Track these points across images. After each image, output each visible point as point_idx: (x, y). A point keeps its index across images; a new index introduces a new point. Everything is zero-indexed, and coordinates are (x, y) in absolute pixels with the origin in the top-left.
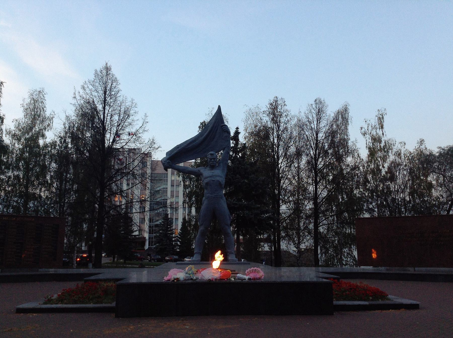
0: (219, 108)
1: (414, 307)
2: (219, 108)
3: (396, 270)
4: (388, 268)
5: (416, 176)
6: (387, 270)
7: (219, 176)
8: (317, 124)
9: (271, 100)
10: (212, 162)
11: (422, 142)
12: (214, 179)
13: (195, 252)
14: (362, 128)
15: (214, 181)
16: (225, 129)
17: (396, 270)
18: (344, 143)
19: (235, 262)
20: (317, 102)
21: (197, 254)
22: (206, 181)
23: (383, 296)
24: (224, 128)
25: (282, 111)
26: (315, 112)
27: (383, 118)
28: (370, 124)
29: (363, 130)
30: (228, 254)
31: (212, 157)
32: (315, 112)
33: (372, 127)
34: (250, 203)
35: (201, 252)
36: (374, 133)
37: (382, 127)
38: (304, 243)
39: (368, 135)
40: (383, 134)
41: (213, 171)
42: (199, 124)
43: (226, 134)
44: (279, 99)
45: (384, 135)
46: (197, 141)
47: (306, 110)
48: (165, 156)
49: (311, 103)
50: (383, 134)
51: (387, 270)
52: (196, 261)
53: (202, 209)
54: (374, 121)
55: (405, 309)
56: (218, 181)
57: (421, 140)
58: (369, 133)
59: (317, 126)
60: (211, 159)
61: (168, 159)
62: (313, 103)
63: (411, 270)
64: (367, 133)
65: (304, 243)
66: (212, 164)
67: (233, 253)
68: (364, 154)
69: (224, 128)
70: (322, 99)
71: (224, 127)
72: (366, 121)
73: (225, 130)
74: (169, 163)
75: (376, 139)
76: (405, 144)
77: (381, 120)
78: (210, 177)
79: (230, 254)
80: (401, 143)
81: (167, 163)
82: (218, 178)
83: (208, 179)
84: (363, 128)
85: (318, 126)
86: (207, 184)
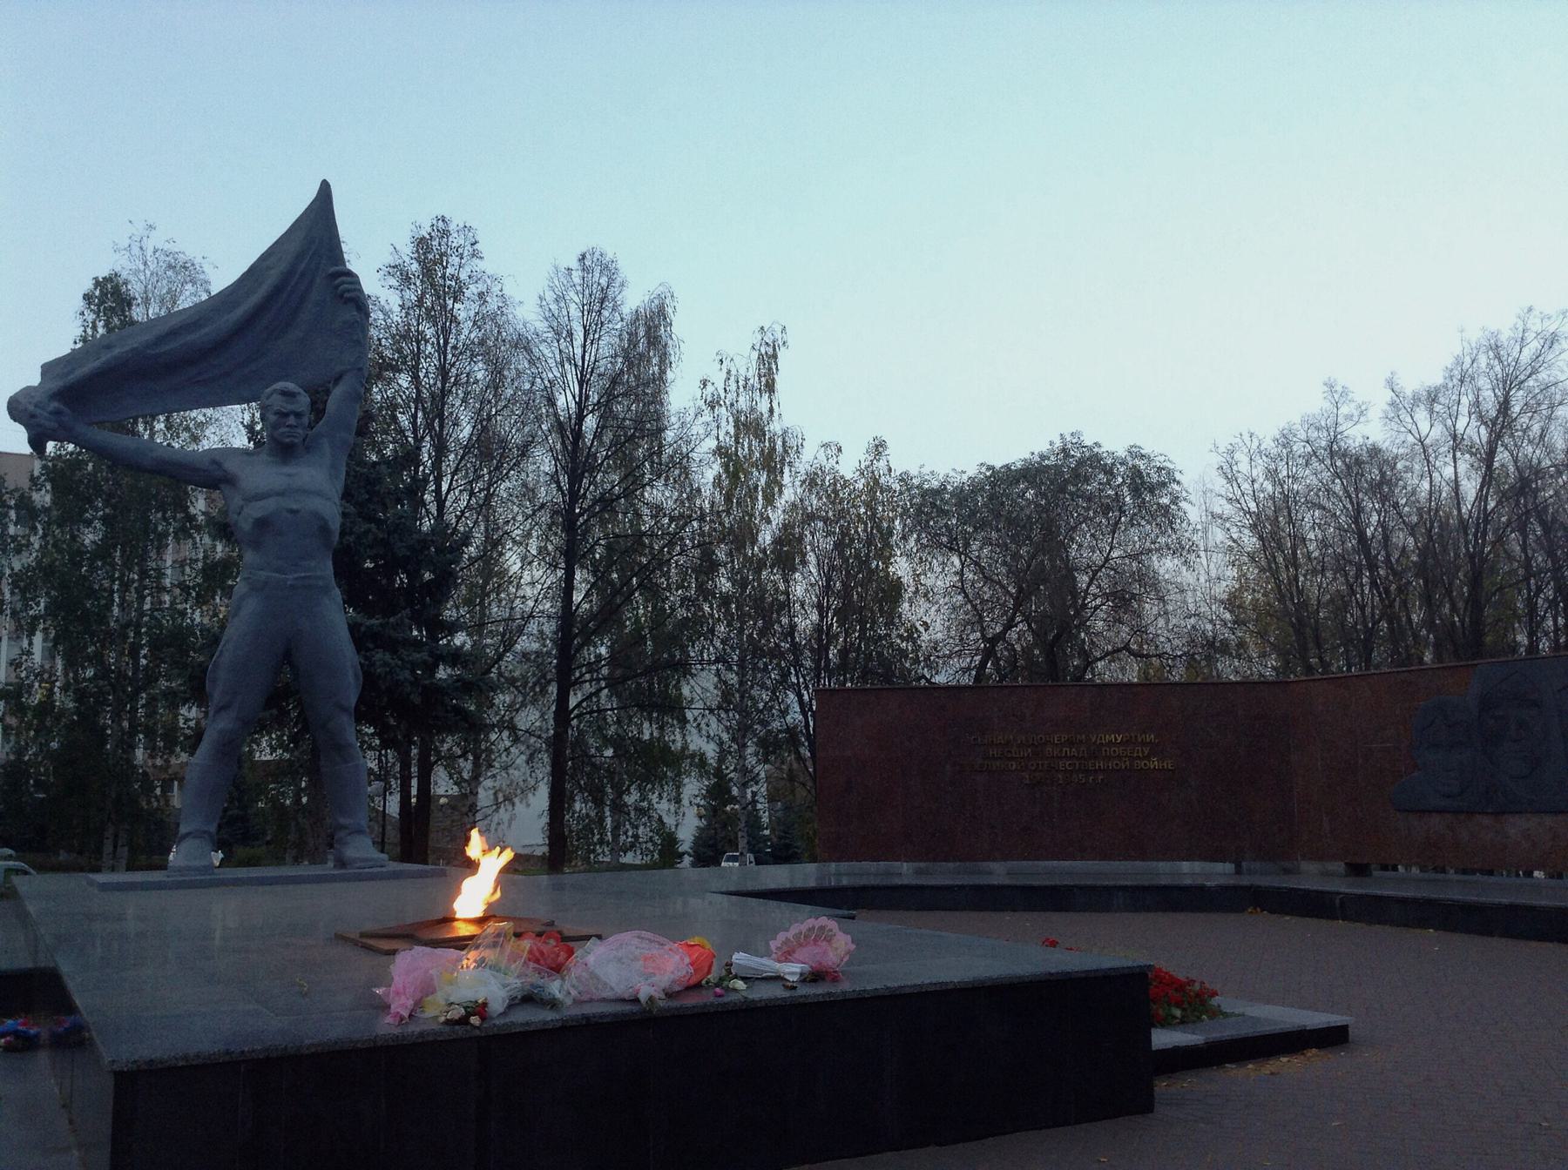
0: (325, 191)
1: (1334, 1038)
2: (325, 191)
3: (944, 874)
4: (922, 865)
5: (858, 556)
6: (918, 872)
7: (319, 494)
8: (584, 346)
9: (423, 225)
10: (287, 429)
11: (879, 448)
12: (295, 507)
13: (183, 830)
14: (704, 383)
15: (292, 512)
16: (349, 291)
17: (944, 874)
18: (650, 423)
19: (379, 869)
20: (588, 263)
21: (194, 837)
22: (256, 511)
23: (1195, 1003)
24: (343, 283)
25: (463, 276)
26: (577, 300)
27: (775, 356)
28: (734, 372)
29: (710, 388)
30: (341, 834)
31: (290, 407)
32: (577, 300)
33: (738, 382)
34: (392, 620)
35: (213, 828)
36: (743, 403)
37: (770, 387)
38: (494, 776)
39: (724, 409)
40: (771, 411)
41: (286, 470)
42: (88, 285)
43: (351, 314)
44: (452, 227)
45: (776, 414)
46: (204, 331)
47: (546, 288)
48: (35, 379)
49: (563, 264)
50: (771, 411)
51: (918, 872)
52: (197, 869)
53: (227, 641)
54: (747, 366)
55: (1318, 1047)
56: (317, 515)
57: (876, 442)
58: (728, 403)
59: (584, 352)
60: (286, 415)
61: (59, 395)
62: (574, 264)
63: (998, 872)
64: (722, 402)
65: (494, 776)
66: (289, 436)
67: (360, 832)
68: (708, 474)
69: (343, 283)
70: (610, 256)
71: (344, 278)
72: (721, 361)
73: (346, 295)
74: (57, 413)
75: (750, 426)
76: (840, 450)
77: (768, 361)
78: (280, 494)
79: (350, 834)
80: (826, 446)
81: (51, 413)
82: (316, 504)
83: (270, 505)
84: (709, 384)
85: (587, 354)
86: (262, 524)
